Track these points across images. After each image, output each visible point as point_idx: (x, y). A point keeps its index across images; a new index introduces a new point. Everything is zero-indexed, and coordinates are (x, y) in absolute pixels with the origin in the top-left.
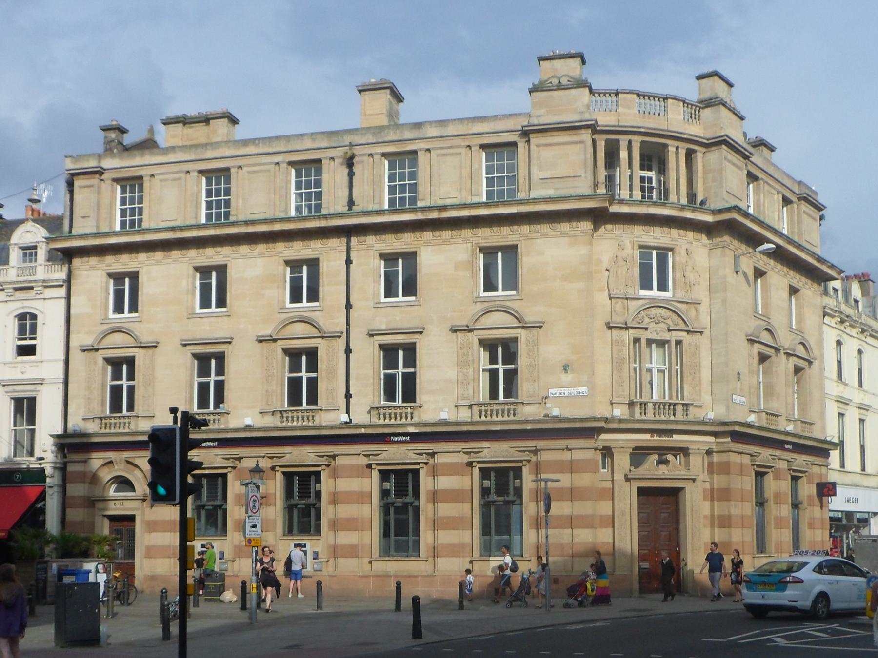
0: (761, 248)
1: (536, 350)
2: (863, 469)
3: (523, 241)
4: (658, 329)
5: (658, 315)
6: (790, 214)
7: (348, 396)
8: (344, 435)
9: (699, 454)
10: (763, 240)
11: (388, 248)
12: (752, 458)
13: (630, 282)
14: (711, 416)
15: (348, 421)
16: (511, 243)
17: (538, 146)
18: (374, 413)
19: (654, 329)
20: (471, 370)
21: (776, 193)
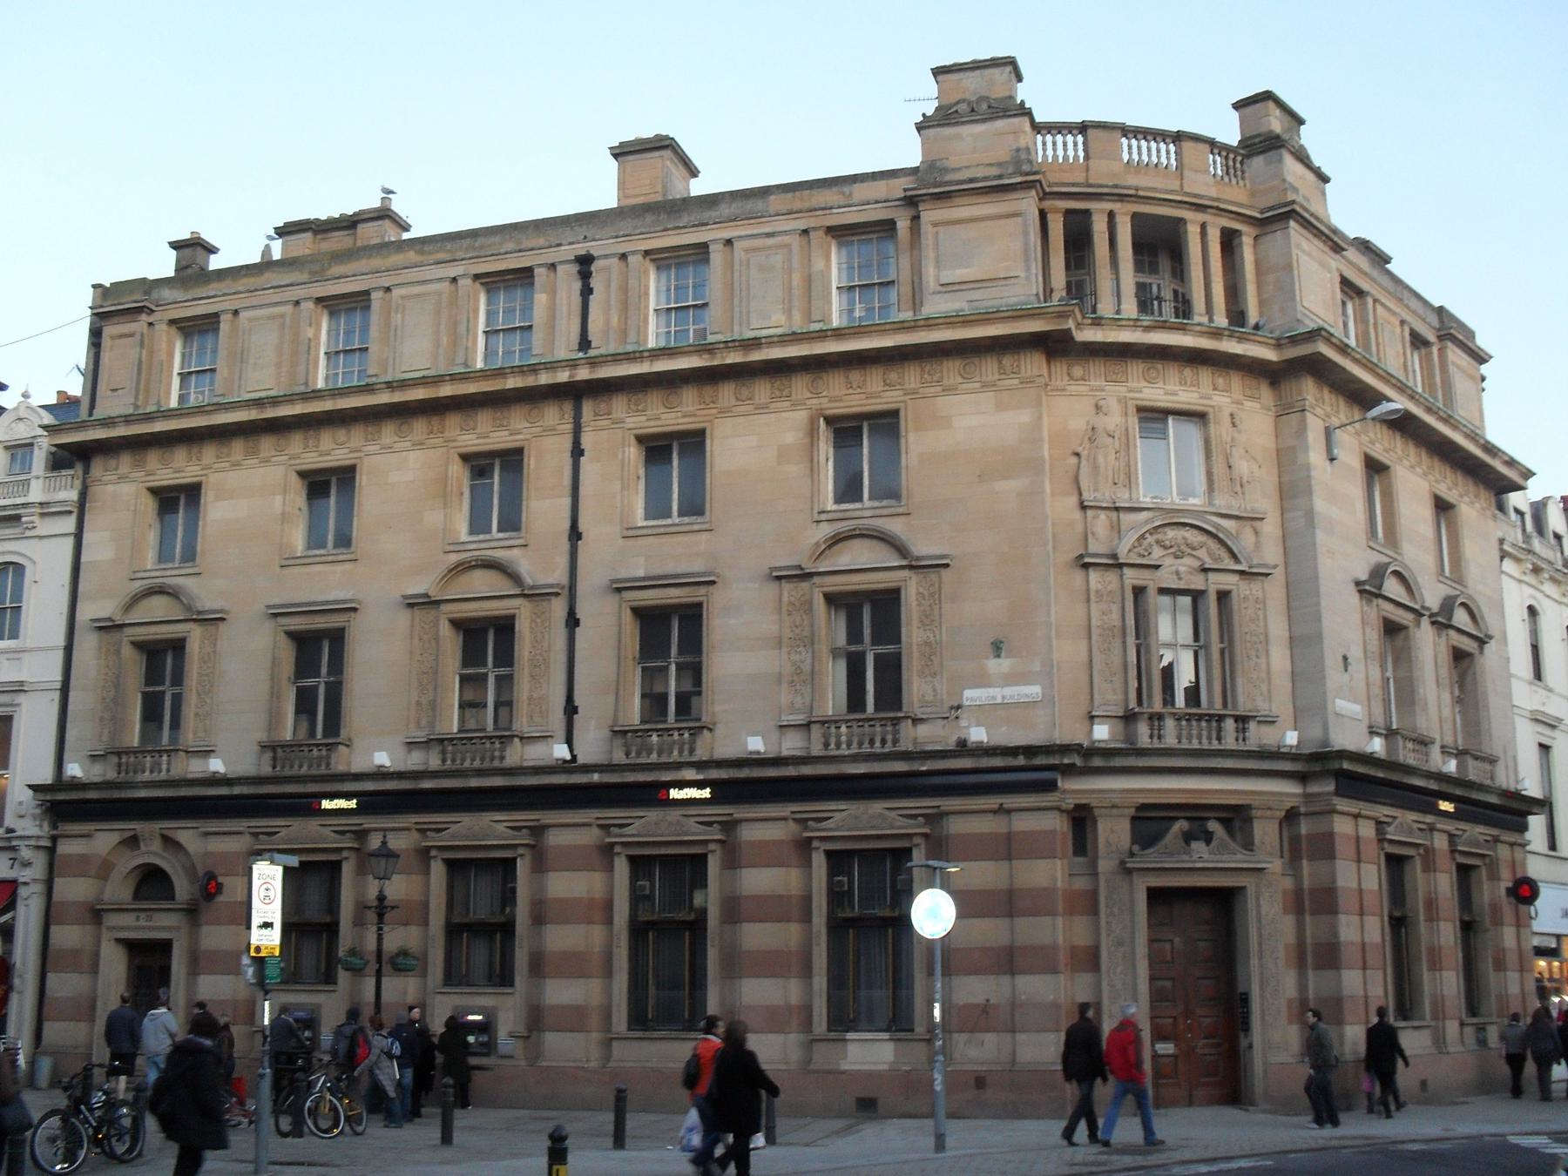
0: (1375, 412)
1: (936, 612)
2: (1553, 847)
3: (909, 402)
4: (1182, 569)
5: (1180, 537)
6: (1426, 363)
7: (571, 709)
8: (560, 785)
9: (1272, 818)
10: (1379, 398)
11: (652, 423)
12: (1380, 826)
13: (1122, 476)
14: (1292, 738)
16: (886, 407)
17: (935, 225)
18: (618, 742)
19: (1174, 568)
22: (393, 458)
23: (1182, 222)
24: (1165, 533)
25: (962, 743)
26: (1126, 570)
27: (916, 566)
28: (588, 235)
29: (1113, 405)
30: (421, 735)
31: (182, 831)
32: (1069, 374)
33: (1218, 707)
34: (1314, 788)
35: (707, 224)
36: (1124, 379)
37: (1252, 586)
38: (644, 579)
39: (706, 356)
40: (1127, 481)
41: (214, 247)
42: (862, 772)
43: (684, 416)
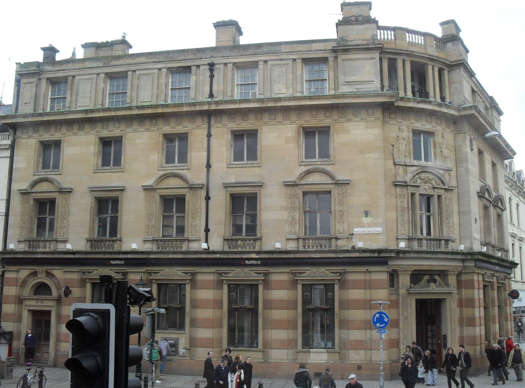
4: (427, 187)
5: (427, 178)
7: (207, 230)
13: (408, 154)
14: (462, 247)
15: (207, 248)
18: (226, 243)
20: (298, 214)
21: (482, 102)
22: (137, 134)
23: (427, 64)
24: (422, 175)
25: (353, 247)
26: (409, 187)
27: (338, 183)
28: (212, 55)
29: (404, 128)
30: (150, 238)
31: (54, 270)
32: (390, 117)
33: (437, 236)
34: (467, 264)
35: (258, 54)
36: (408, 119)
37: (448, 194)
38: (235, 183)
39: (260, 103)
40: (409, 155)
41: (58, 50)
42: (318, 257)
43: (250, 124)
